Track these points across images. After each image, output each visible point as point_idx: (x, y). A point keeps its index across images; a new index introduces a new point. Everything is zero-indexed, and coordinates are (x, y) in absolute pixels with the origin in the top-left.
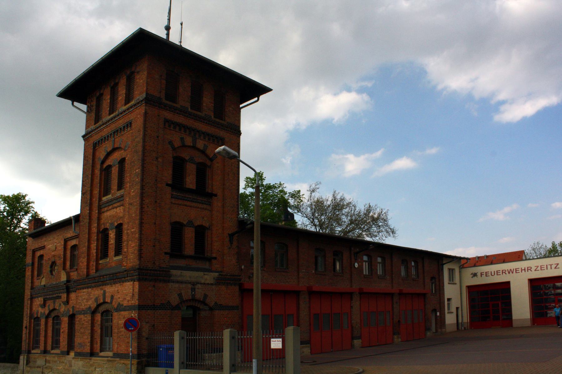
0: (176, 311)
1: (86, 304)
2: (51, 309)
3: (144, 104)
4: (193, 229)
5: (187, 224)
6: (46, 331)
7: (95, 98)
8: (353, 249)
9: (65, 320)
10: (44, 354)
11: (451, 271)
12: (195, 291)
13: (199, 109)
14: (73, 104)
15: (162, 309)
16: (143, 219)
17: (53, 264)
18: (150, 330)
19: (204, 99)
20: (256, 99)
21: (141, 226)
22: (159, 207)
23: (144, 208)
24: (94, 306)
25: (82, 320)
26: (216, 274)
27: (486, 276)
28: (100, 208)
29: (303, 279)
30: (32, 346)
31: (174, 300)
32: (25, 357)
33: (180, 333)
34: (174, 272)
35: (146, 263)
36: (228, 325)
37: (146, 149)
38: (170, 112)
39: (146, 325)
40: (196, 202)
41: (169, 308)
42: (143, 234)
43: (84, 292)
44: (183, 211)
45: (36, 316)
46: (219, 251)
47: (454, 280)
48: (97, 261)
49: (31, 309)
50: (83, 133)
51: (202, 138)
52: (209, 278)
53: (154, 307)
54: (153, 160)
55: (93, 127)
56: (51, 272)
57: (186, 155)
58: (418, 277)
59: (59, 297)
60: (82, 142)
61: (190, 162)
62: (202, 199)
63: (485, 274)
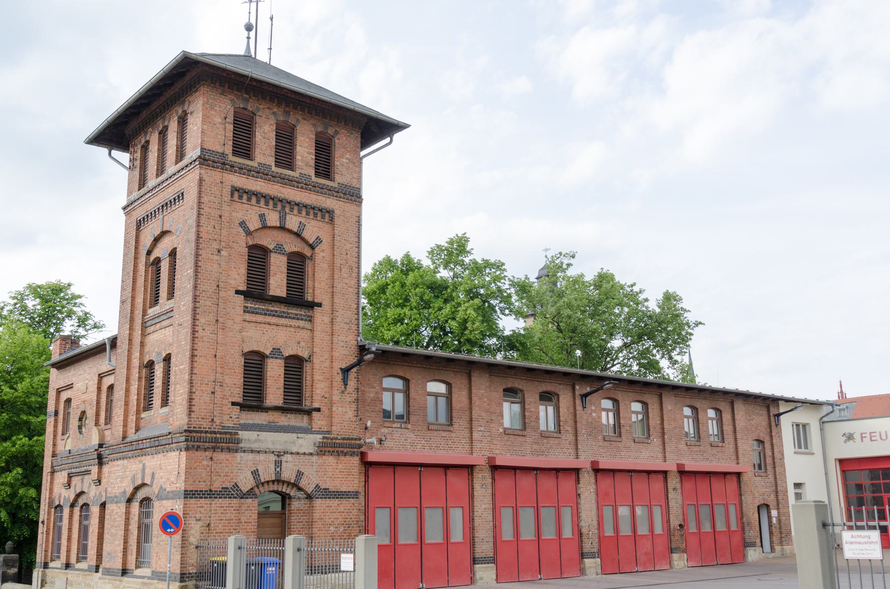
0: (250, 501)
1: (120, 485)
2: (78, 491)
3: (198, 166)
4: (281, 362)
6: (70, 529)
7: (139, 147)
8: (577, 387)
9: (95, 510)
10: (66, 569)
11: (801, 429)
12: (281, 466)
13: (290, 166)
14: (110, 154)
16: (196, 350)
17: (83, 416)
18: (203, 533)
19: (298, 149)
20: (388, 140)
21: (192, 361)
22: (223, 329)
23: (197, 332)
24: (130, 490)
25: (114, 513)
26: (319, 438)
27: (871, 440)
28: (144, 327)
29: (480, 443)
31: (246, 482)
32: (40, 573)
33: (294, 539)
34: (243, 435)
36: (338, 524)
37: (202, 238)
38: (241, 175)
39: (196, 524)
40: (286, 317)
41: (235, 495)
42: (196, 374)
43: (118, 466)
44: (263, 333)
45: (57, 503)
46: (326, 398)
47: (809, 447)
48: (138, 412)
49: (51, 490)
50: (125, 203)
51: (295, 212)
52: (307, 443)
53: (210, 494)
54: (213, 254)
55: (136, 195)
56: (80, 427)
57: (268, 240)
58: (723, 440)
59: (88, 472)
60: (123, 218)
62: (296, 312)
63: (868, 436)
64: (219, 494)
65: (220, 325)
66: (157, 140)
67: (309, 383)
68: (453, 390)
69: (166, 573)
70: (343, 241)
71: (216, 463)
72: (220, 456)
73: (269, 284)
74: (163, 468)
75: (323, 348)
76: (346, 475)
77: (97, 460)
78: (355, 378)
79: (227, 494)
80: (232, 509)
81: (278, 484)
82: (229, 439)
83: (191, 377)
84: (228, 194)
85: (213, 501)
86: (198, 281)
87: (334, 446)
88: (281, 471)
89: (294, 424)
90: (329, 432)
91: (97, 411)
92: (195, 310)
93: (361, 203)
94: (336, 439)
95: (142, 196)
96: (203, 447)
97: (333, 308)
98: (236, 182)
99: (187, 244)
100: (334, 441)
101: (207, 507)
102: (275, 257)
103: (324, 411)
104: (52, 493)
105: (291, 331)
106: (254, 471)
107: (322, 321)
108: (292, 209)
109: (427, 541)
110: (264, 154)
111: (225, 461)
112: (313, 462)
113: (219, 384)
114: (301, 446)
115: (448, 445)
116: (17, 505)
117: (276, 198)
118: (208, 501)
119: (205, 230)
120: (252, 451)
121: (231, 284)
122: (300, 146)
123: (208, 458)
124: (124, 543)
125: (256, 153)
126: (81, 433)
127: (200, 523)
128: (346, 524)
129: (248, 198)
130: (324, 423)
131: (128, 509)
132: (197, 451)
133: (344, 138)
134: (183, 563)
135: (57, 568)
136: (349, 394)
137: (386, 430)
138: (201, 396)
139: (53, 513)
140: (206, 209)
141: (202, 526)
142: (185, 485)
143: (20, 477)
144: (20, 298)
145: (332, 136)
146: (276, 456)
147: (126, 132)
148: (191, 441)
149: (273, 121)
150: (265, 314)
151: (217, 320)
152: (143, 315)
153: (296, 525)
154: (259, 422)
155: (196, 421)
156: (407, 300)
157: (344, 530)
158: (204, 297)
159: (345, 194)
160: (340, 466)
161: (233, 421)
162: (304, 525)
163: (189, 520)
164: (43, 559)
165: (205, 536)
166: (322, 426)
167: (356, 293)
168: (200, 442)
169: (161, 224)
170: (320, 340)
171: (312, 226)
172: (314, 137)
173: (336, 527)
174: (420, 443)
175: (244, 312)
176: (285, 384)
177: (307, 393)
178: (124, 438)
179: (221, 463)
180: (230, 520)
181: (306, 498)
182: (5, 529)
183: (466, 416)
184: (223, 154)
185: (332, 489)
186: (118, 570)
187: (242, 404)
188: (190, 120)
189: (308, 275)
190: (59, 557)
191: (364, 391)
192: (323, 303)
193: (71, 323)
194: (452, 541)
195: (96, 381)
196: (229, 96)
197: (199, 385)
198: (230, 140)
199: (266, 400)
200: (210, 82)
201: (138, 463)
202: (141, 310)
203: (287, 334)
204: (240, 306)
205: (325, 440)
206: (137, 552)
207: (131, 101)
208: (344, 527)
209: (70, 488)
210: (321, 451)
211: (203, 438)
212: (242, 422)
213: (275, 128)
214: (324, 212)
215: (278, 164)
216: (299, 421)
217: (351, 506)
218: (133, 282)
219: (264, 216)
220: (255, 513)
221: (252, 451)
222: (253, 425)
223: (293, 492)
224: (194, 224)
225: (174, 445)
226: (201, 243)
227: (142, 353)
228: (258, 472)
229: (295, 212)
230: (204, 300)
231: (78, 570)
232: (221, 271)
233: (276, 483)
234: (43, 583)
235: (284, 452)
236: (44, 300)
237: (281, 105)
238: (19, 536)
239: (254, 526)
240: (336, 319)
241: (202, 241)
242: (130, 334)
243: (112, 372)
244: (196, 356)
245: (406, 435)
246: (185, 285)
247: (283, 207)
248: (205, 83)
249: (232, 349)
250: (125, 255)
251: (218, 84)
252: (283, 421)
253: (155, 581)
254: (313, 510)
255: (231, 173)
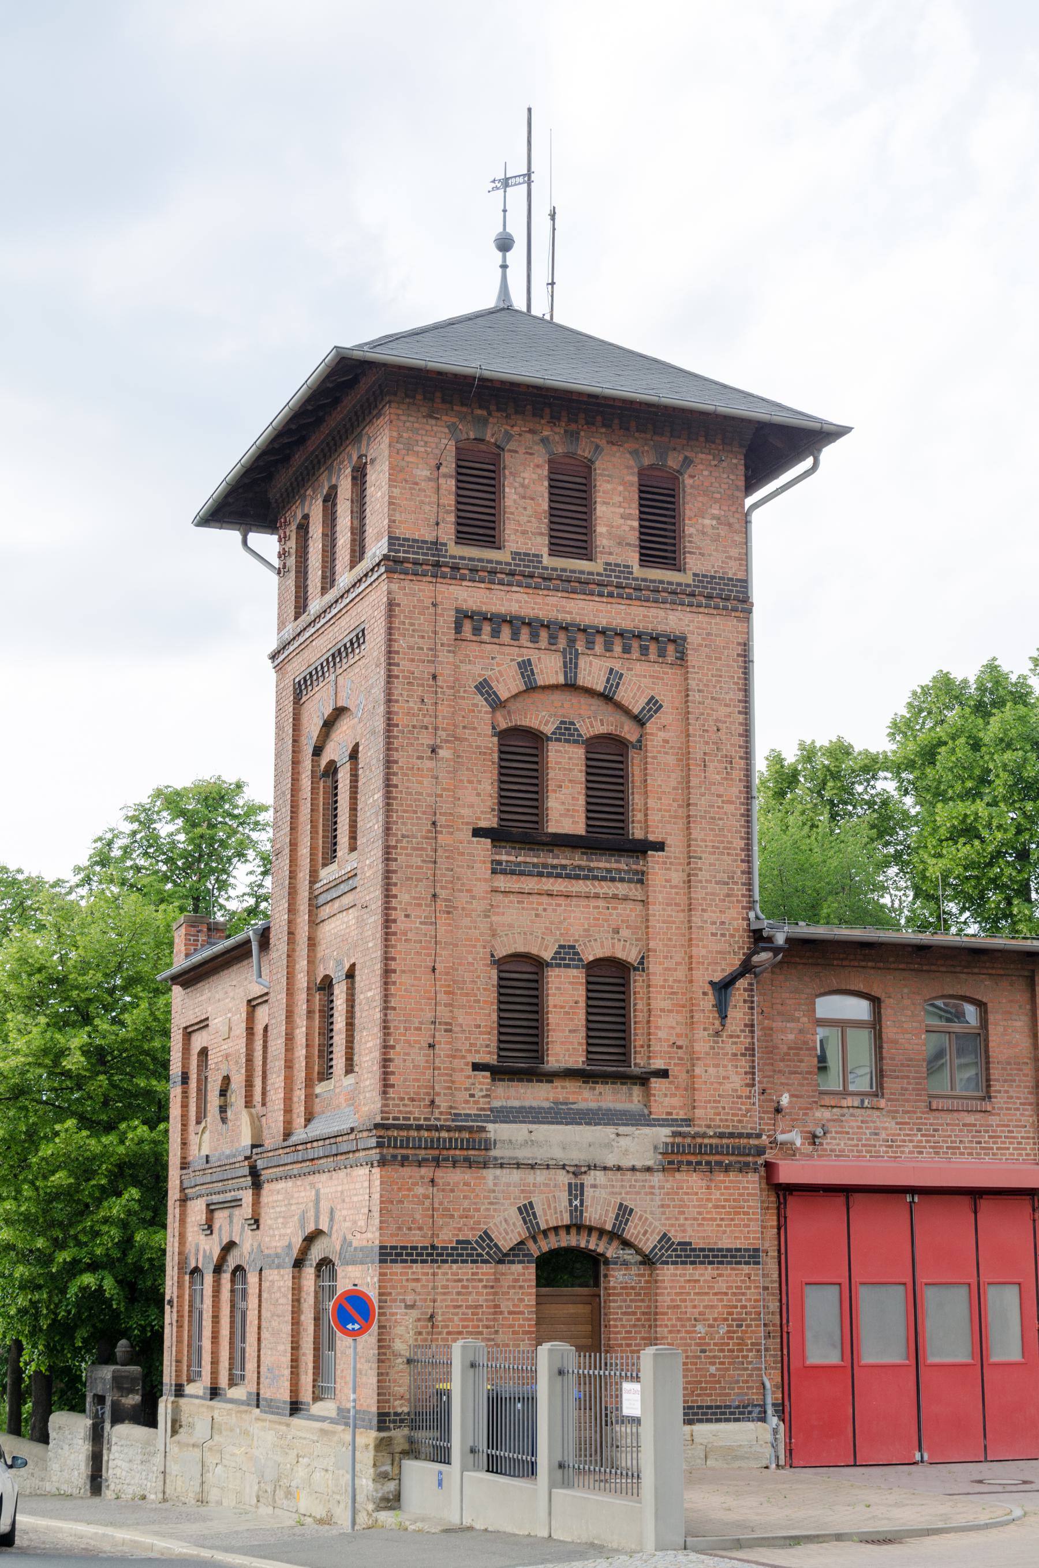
0: (517, 1268)
1: (283, 1231)
2: (225, 1241)
3: (384, 576)
4: (578, 975)
5: (553, 958)
6: (216, 1319)
7: (294, 527)
10: (211, 1399)
12: (582, 1194)
13: (584, 549)
14: (245, 542)
15: (463, 1262)
16: (394, 959)
18: (420, 1333)
19: (601, 510)
20: (809, 462)
21: (386, 983)
22: (448, 913)
23: (395, 921)
24: (297, 1242)
25: (276, 1289)
26: (663, 1134)
28: (314, 907)
30: (188, 1371)
32: (169, 1406)
34: (496, 1130)
35: (405, 1105)
36: (715, 1320)
37: (397, 725)
39: (406, 1314)
40: (586, 878)
41: (486, 1257)
42: (394, 1009)
44: (537, 915)
45: (193, 1265)
46: (680, 1047)
48: (309, 1084)
50: (273, 646)
51: (599, 648)
54: (420, 758)
55: (291, 629)
59: (236, 1203)
60: (272, 675)
61: (558, 740)
62: (608, 865)
64: (451, 1255)
65: (441, 904)
66: (321, 515)
67: (641, 1017)
68: (991, 1018)
69: (348, 1411)
70: (708, 701)
71: (443, 1190)
72: (453, 1177)
73: (547, 809)
74: (347, 1200)
75: (670, 940)
76: (729, 1213)
77: (249, 1178)
78: (745, 1001)
79: (468, 1255)
80: (481, 1284)
81: (578, 1233)
82: (468, 1140)
83: (386, 1015)
84: (449, 628)
85: (439, 1267)
86: (392, 817)
87: (700, 1150)
88: (582, 1205)
89: (611, 1105)
90: (688, 1122)
91: (247, 1076)
92: (387, 878)
93: (749, 611)
94: (704, 1135)
95: (299, 634)
96: (415, 1158)
97: (689, 852)
98: (465, 601)
99: (372, 738)
100: (699, 1140)
101: (428, 1281)
102: (557, 751)
103: (676, 1077)
104: (185, 1243)
105: (598, 907)
106: (525, 1206)
107: (666, 881)
108: (590, 644)
109: (932, 1359)
110: (524, 532)
111: (461, 1186)
112: (653, 1187)
113: (443, 1027)
114: (626, 1152)
115: (980, 1143)
116: (134, 1264)
117: (555, 623)
118: (428, 1268)
119: (402, 708)
120: (518, 1164)
121: (462, 817)
122: (604, 503)
123: (427, 1180)
124: (293, 1348)
125: (507, 532)
126: (224, 1120)
127: (415, 1313)
128: (733, 1320)
129: (493, 630)
130: (676, 1101)
131: (297, 1279)
132: (403, 1165)
133: (706, 473)
134: (382, 1392)
135: (197, 1397)
136: (731, 1036)
137: (827, 1114)
138: (408, 1054)
139: (187, 1284)
140: (405, 665)
141: (419, 1320)
142: (381, 1235)
143: (136, 1207)
144: (144, 818)
145: (678, 472)
146: (571, 1175)
147: (270, 496)
148: (389, 1146)
149: (541, 457)
150: (540, 875)
151: (434, 896)
152: (310, 882)
153: (621, 1320)
154: (535, 1104)
155: (398, 1106)
156: (984, 780)
157: (728, 1332)
158: (406, 848)
159: (710, 597)
160: (716, 1194)
161: (476, 1102)
162: (638, 1320)
163: (391, 1307)
164: (174, 1378)
165: (426, 1340)
166: (674, 1108)
167: (742, 815)
168: (407, 1147)
169: (333, 693)
170: (664, 922)
171: (637, 675)
172: (636, 479)
173: (711, 1326)
174: (911, 1141)
175: (494, 872)
176: (588, 1021)
177: (638, 1039)
178: (287, 1135)
179: (452, 1191)
180: (476, 1307)
181: (642, 1263)
182: (116, 1315)
183: (1025, 1075)
184: (436, 543)
185: (698, 1243)
186: (285, 1402)
187: (493, 1066)
188: (372, 476)
189: (633, 782)
190: (199, 1374)
191: (771, 1029)
192: (668, 842)
193: (249, 867)
194: (995, 1358)
195: (244, 1015)
196: (444, 418)
197: (402, 1030)
198: (451, 512)
199: (548, 1055)
200: (403, 395)
201: (308, 1187)
202: (308, 871)
203: (588, 913)
204: (484, 862)
205: (678, 1140)
206: (314, 1368)
207: (262, 444)
208: (729, 1326)
209: (211, 1233)
210: (670, 1163)
211: (414, 1138)
212: (497, 1104)
213: (546, 473)
214: (664, 643)
215: (557, 548)
216: (627, 1098)
217: (743, 1281)
218: (292, 812)
219: (530, 665)
220: (530, 1294)
221: (518, 1166)
222: (521, 1110)
223: (612, 1251)
224: (382, 697)
225: (362, 1154)
226: (396, 737)
227: (311, 961)
228: (532, 1207)
229: (599, 648)
230: (407, 855)
231: (232, 1401)
232: (439, 792)
233: (573, 1231)
234: (176, 1427)
235: (589, 1166)
236: (192, 822)
237: (559, 419)
238: (143, 1329)
239: (530, 1320)
240: (696, 875)
241: (399, 731)
242: (290, 922)
243: (202, 1025)
244: (394, 971)
245: (874, 1122)
246: (371, 824)
247: (571, 642)
248: (392, 398)
249: (471, 952)
250: (278, 755)
251: (419, 397)
252: (585, 1100)
253: (341, 1428)
254: (657, 1288)
255: (453, 582)
